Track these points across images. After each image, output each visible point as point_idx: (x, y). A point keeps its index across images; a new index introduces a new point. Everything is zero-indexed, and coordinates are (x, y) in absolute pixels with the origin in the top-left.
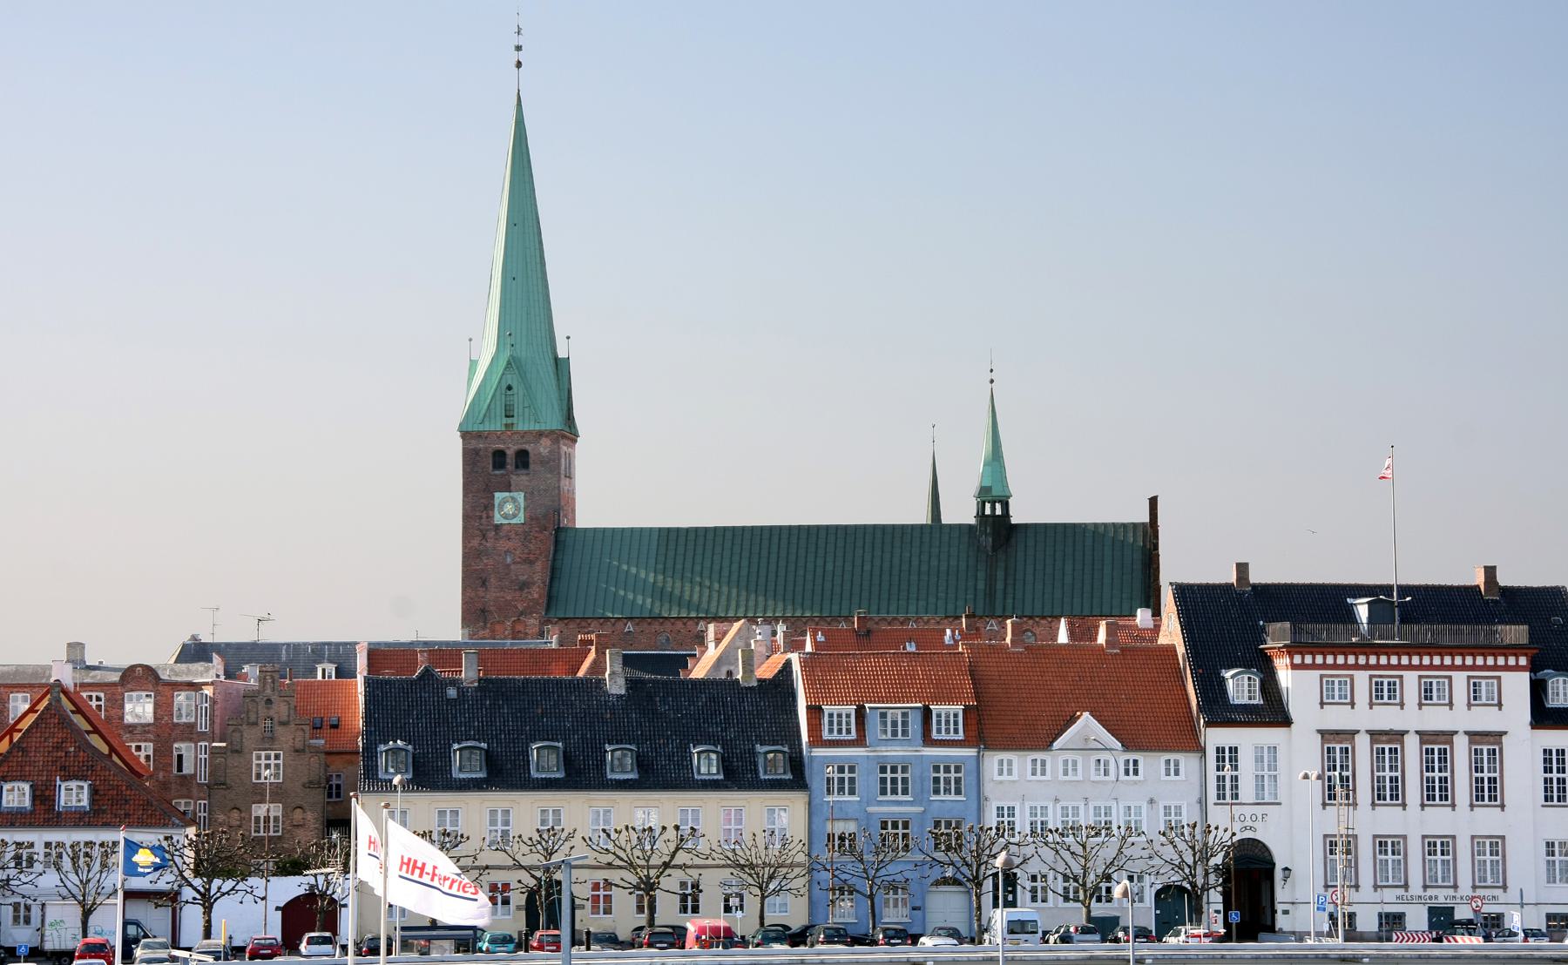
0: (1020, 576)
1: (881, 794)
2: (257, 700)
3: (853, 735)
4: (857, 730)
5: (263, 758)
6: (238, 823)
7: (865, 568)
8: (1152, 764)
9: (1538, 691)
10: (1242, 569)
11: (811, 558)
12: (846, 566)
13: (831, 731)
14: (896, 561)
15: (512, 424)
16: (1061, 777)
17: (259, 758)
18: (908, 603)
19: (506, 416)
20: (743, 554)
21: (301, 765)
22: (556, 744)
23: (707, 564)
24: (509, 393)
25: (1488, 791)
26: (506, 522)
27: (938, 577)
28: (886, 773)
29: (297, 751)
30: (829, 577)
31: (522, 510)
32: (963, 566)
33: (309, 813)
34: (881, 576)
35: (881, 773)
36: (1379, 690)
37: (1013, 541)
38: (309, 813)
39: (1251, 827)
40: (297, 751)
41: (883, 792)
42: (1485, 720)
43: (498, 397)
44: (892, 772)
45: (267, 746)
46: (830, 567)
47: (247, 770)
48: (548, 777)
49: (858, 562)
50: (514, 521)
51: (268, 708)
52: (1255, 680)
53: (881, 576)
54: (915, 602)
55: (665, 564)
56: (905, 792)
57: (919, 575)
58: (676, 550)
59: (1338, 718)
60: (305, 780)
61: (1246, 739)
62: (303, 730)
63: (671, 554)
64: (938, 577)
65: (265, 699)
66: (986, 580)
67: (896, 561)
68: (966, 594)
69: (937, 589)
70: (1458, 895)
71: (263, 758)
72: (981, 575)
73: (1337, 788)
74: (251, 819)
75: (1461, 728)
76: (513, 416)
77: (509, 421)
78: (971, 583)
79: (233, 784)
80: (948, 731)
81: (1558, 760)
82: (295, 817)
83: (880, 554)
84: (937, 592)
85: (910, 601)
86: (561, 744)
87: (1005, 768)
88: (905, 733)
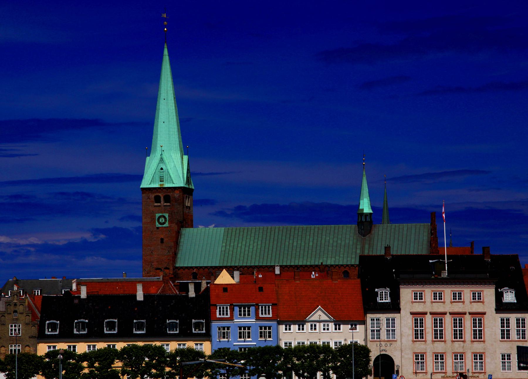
0: (375, 247)
1: (239, 338)
2: (11, 304)
3: (229, 316)
4: (272, 313)
5: (13, 326)
6: (4, 352)
7: (310, 244)
8: (345, 328)
9: (499, 296)
10: (387, 249)
11: (287, 240)
12: (302, 243)
13: (220, 314)
14: (323, 241)
15: (163, 184)
16: (310, 331)
17: (12, 326)
18: (327, 259)
19: (160, 181)
20: (259, 239)
21: (28, 329)
22: (202, 321)
23: (244, 243)
24: (161, 171)
25: (478, 335)
26: (161, 226)
27: (340, 248)
28: (16, 327)
29: (26, 324)
30: (294, 248)
31: (167, 221)
32: (351, 243)
33: (31, 348)
34: (316, 248)
35: (239, 330)
36: (454, 296)
37: (373, 232)
38: (31, 348)
39: (385, 350)
40: (26, 324)
41: (240, 337)
42: (477, 308)
43: (157, 173)
44: (14, 327)
45: (15, 322)
46: (295, 244)
47: (7, 331)
48: (82, 333)
49: (307, 242)
50: (164, 226)
51: (15, 307)
52: (387, 293)
53: (316, 248)
54: (330, 259)
55: (226, 243)
56: (249, 337)
57: (332, 247)
58: (231, 237)
59: (419, 308)
60: (30, 335)
61: (383, 317)
62: (29, 316)
63: (229, 239)
64: (340, 248)
65: (14, 304)
66: (360, 249)
67: (323, 241)
68: (352, 255)
69: (340, 253)
70: (446, 376)
71: (13, 326)
72: (359, 247)
73: (419, 335)
74: (9, 350)
75: (467, 311)
76: (163, 181)
77: (162, 183)
78: (354, 250)
79: (2, 337)
80: (223, 314)
81: (522, 323)
82: (26, 349)
83: (316, 238)
84: (340, 254)
85: (328, 258)
86: (58, 322)
87: (313, 327)
88: (249, 315)
